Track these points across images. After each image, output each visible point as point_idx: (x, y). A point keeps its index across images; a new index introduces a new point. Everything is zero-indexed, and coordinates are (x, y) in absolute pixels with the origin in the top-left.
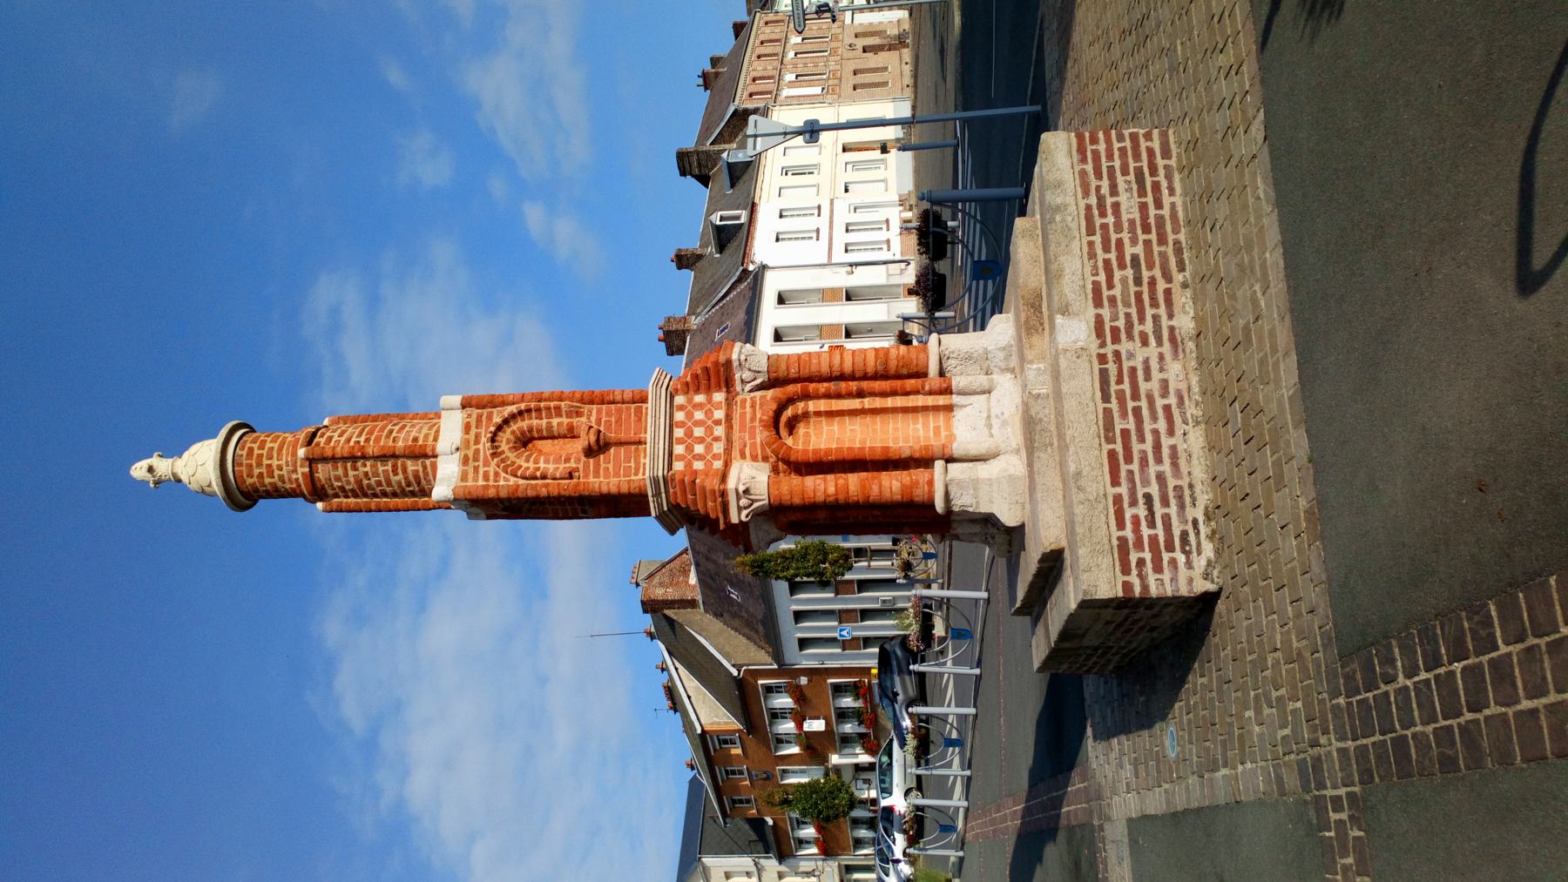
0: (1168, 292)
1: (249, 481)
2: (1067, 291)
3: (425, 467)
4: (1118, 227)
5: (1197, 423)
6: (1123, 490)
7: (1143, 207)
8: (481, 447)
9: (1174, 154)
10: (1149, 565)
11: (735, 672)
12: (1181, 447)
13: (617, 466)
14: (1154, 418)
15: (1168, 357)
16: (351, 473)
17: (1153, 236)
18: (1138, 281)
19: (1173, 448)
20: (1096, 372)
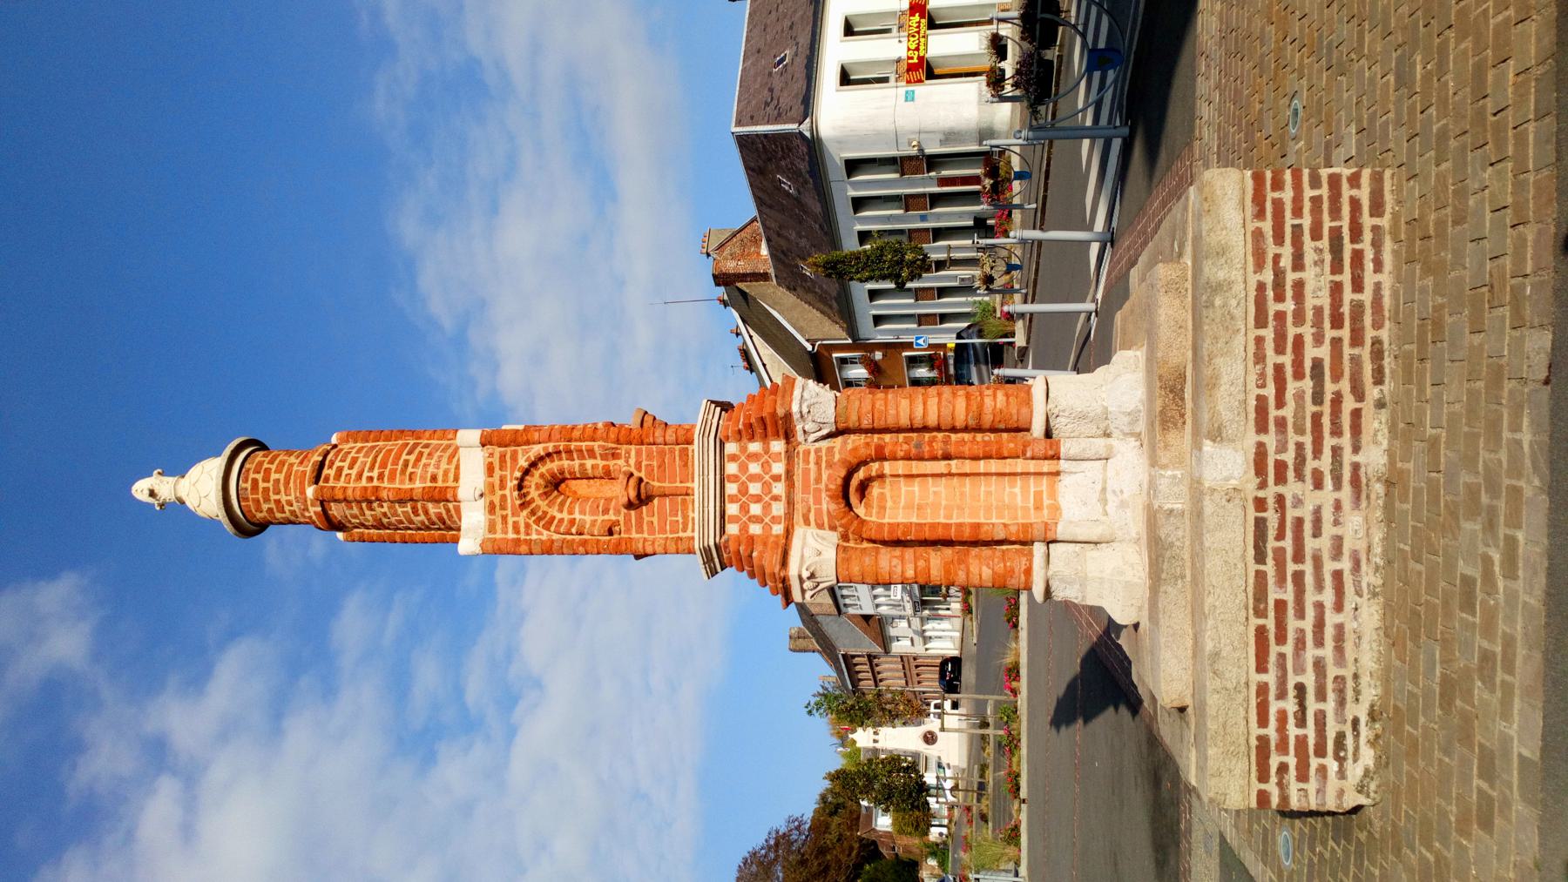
0: (1356, 414)
1: (259, 515)
2: (1221, 407)
3: (448, 511)
4: (1299, 317)
5: (1375, 595)
6: (1270, 678)
7: (1336, 289)
8: (507, 492)
9: (1388, 209)
10: (1292, 772)
11: (809, 348)
12: (1350, 626)
13: (663, 521)
14: (1319, 586)
15: (1347, 504)
16: (368, 513)
17: (1345, 333)
18: (1318, 398)
19: (1340, 628)
20: (1251, 522)
